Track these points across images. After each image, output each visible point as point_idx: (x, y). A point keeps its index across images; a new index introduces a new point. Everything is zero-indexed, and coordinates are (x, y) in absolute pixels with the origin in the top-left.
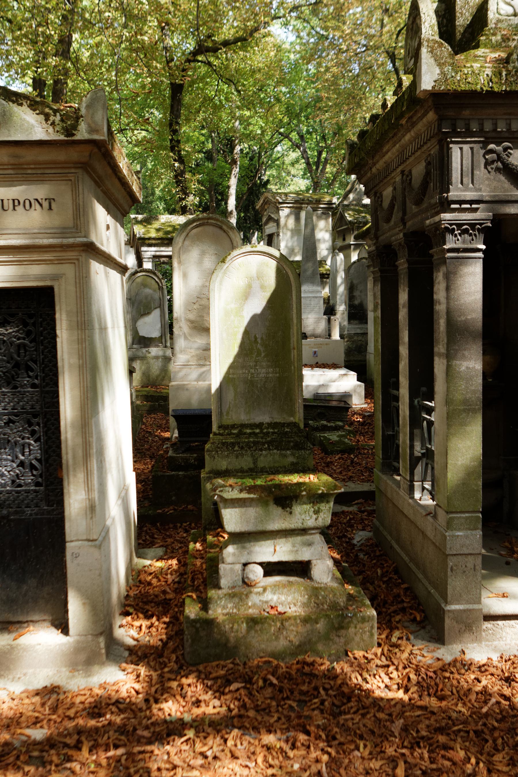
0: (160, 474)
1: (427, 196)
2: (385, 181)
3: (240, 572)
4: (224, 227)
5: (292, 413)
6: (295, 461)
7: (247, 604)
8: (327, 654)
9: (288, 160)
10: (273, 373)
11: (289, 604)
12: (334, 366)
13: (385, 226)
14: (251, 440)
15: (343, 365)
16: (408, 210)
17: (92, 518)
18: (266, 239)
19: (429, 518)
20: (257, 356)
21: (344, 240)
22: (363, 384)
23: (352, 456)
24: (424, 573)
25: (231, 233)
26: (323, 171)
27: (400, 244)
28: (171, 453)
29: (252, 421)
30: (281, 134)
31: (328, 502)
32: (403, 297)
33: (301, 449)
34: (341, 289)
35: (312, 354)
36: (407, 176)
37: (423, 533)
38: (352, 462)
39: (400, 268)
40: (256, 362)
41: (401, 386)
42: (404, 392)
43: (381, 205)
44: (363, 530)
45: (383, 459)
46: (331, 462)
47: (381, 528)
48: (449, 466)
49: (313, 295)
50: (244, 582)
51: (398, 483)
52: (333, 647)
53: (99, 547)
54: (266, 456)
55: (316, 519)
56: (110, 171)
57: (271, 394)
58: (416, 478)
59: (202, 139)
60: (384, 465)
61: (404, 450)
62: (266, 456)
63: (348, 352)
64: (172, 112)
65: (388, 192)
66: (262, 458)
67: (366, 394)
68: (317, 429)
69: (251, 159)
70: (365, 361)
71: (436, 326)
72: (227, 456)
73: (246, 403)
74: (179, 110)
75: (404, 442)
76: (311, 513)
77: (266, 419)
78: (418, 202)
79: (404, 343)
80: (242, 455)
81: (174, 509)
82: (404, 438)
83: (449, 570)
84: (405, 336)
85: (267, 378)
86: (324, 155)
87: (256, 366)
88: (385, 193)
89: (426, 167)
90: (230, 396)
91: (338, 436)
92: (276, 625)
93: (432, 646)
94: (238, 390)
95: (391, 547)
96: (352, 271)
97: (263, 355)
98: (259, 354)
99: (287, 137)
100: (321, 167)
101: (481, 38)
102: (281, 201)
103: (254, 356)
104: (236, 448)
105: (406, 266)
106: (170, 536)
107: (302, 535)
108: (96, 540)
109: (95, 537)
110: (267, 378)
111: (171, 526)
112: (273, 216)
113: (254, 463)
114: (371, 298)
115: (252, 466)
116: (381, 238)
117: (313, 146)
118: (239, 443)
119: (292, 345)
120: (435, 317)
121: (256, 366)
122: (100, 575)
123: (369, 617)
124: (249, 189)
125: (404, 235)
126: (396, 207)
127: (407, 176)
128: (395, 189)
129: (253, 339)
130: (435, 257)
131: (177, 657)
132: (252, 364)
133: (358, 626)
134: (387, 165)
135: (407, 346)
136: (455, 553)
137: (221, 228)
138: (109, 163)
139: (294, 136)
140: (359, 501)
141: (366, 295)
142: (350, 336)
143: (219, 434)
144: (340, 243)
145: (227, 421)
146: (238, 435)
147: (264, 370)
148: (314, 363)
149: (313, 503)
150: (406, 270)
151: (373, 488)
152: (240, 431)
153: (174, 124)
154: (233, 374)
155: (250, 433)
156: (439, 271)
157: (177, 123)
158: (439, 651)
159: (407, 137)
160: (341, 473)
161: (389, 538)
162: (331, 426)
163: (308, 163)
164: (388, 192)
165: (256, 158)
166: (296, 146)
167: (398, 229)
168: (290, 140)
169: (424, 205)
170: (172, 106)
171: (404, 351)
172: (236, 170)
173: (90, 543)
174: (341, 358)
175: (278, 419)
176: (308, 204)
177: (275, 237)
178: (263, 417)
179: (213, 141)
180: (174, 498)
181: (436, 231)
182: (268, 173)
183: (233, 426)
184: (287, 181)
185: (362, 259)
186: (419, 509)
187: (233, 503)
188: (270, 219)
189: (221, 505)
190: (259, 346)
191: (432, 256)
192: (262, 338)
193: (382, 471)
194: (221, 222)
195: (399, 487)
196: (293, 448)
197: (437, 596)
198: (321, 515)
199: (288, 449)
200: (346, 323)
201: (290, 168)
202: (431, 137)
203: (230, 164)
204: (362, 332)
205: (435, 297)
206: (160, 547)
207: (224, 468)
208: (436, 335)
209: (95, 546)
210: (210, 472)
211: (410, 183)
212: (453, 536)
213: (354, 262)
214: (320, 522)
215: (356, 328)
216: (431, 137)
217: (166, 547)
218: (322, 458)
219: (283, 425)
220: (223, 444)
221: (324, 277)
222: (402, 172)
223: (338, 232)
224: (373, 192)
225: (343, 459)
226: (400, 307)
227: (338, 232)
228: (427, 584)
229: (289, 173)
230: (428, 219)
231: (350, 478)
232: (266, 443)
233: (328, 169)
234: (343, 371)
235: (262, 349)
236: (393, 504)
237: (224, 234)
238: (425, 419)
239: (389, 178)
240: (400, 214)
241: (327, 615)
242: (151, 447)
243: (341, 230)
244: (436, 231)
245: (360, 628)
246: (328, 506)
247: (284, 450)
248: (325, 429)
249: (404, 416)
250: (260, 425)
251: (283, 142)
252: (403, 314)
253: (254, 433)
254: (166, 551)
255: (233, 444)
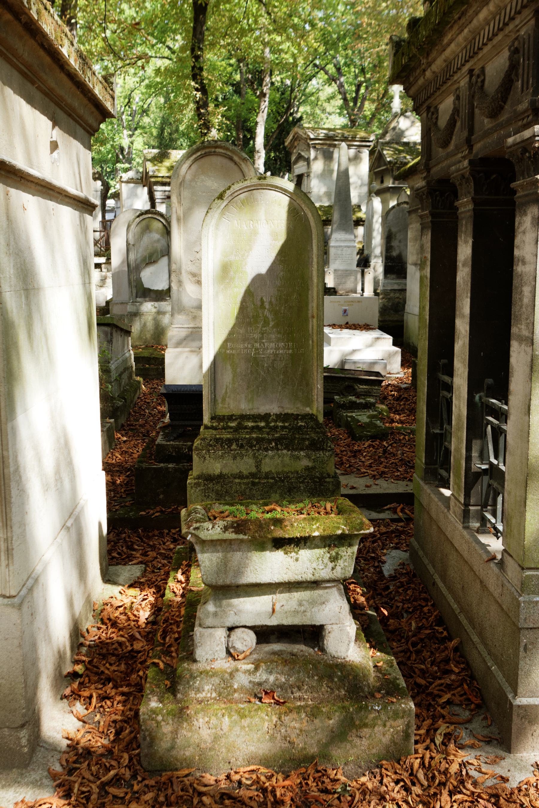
0: (144, 465)
1: (509, 102)
2: (444, 88)
3: (223, 639)
4: (236, 158)
5: (308, 402)
6: (310, 464)
7: (231, 686)
8: (343, 760)
9: (323, 96)
10: (284, 348)
11: (291, 686)
12: (367, 327)
13: (441, 152)
14: (254, 436)
15: (377, 326)
16: (477, 127)
17: (8, 565)
18: (295, 180)
19: (492, 565)
20: (263, 326)
21: (382, 182)
22: (400, 350)
23: (385, 443)
24: (481, 635)
25: (243, 166)
26: (361, 108)
27: (463, 176)
28: (160, 440)
29: (255, 412)
30: (315, 65)
31: (350, 545)
32: (465, 251)
33: (319, 449)
34: (377, 239)
35: (341, 313)
36: (477, 78)
37: (481, 582)
38: (385, 452)
39: (462, 210)
40: (263, 334)
41: (455, 373)
42: (460, 380)
43: (436, 124)
44: (396, 548)
45: (426, 463)
46: (360, 451)
47: (421, 553)
48: (528, 502)
49: (343, 245)
50: (228, 652)
51: (447, 500)
52: (351, 752)
53: (20, 607)
54: (272, 458)
55: (333, 569)
56: (48, 60)
57: (282, 377)
58: (472, 501)
59: (230, 69)
60: (426, 471)
61: (458, 461)
62: (272, 458)
63: (383, 311)
64: (194, 35)
65: (446, 106)
66: (267, 460)
67: (402, 361)
68: (344, 406)
69: (283, 94)
70: (402, 321)
71: (515, 296)
72: (222, 457)
73: (248, 387)
74: (202, 33)
75: (458, 450)
76: (326, 560)
77: (273, 408)
78: (494, 114)
79: (463, 316)
80: (242, 456)
81: (161, 511)
82: (458, 442)
83: (522, 649)
84: (464, 306)
85: (276, 355)
86: (362, 90)
87: (262, 338)
88: (442, 107)
89: (510, 58)
90: (226, 377)
91: (368, 417)
92: (271, 720)
93: (492, 751)
94: (238, 370)
95: (434, 584)
96: (390, 217)
97: (272, 324)
98: (266, 323)
99: (323, 69)
100: (359, 104)
101: (188, 539)
102: (312, 136)
103: (260, 325)
104: (234, 447)
105: (471, 207)
106: (153, 548)
107: (313, 589)
108: (14, 597)
109: (13, 593)
110: (276, 355)
111: (156, 532)
112: (303, 154)
113: (257, 467)
114: (416, 249)
115: (254, 470)
116: (434, 170)
117: (351, 80)
118: (237, 440)
119: (310, 312)
120: (515, 282)
121: (262, 338)
122: (20, 646)
123: (404, 712)
124: (279, 126)
125: (471, 162)
126: (458, 124)
127: (478, 76)
128: (458, 98)
129: (259, 303)
130: (520, 193)
131: (131, 759)
132: (256, 336)
133: (388, 724)
134: (449, 63)
135: (467, 320)
136: (531, 626)
137: (231, 159)
138: (42, 46)
139: (331, 68)
140: (392, 505)
141: (406, 246)
142: (386, 293)
143: (212, 428)
144: (377, 186)
145: (223, 410)
146: (236, 430)
147: (272, 345)
148: (343, 323)
149: (329, 546)
150: (471, 213)
151: (409, 490)
152: (239, 423)
153: (196, 49)
154: (232, 349)
155: (253, 427)
156: (525, 214)
157: (200, 49)
158: (503, 763)
159: (483, 15)
160: (370, 466)
161: (431, 570)
162: (361, 404)
163: (345, 99)
164: (446, 106)
165: (289, 93)
166: (332, 79)
167: (460, 155)
168: (326, 73)
169: (504, 117)
170: (195, 28)
171: (462, 326)
172: (265, 105)
173: (6, 601)
174: (374, 317)
175: (290, 409)
176: (342, 141)
177: (305, 178)
178: (271, 407)
179: (241, 72)
180: (161, 496)
181: (523, 153)
182: (302, 109)
183: (231, 418)
184: (322, 119)
185: (402, 203)
186: (477, 547)
187: (215, 546)
188: (300, 157)
189: (197, 548)
190: (266, 312)
191: (514, 192)
192: (271, 303)
193: (424, 479)
194: (231, 151)
195: (448, 508)
196: (308, 448)
197: (500, 677)
198: (341, 562)
199: (302, 449)
200: (381, 277)
201: (326, 105)
202: (524, 7)
203: (258, 97)
204: (400, 288)
205: (516, 252)
206: (138, 564)
207: (217, 472)
208: (515, 309)
209: (13, 606)
210: (199, 477)
211: (482, 86)
212: (530, 602)
213: (393, 207)
214: (338, 573)
215: (394, 284)
216: (524, 7)
217: (145, 563)
218: (348, 446)
219: (296, 417)
220: (217, 440)
221: (359, 222)
222: (471, 72)
223: (376, 173)
224: (425, 106)
225: (374, 447)
226: (460, 264)
227: (376, 173)
228: (485, 654)
229: (324, 111)
230: (510, 136)
231: (382, 475)
232: (273, 440)
233: (367, 104)
234: (377, 333)
235: (270, 317)
236: (439, 527)
237: (235, 167)
238: (489, 422)
239: (450, 83)
240: (465, 134)
241: (344, 708)
242: (146, 422)
243: (379, 169)
244: (523, 153)
245: (391, 727)
246: (350, 550)
247: (296, 450)
248: (353, 406)
249: (459, 416)
250: (266, 417)
251: (319, 75)
252: (463, 275)
253: (258, 427)
254: (146, 570)
255: (230, 442)
